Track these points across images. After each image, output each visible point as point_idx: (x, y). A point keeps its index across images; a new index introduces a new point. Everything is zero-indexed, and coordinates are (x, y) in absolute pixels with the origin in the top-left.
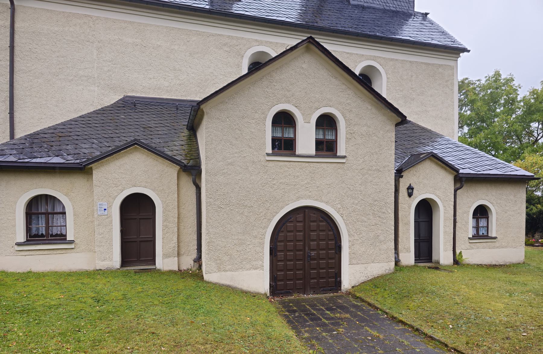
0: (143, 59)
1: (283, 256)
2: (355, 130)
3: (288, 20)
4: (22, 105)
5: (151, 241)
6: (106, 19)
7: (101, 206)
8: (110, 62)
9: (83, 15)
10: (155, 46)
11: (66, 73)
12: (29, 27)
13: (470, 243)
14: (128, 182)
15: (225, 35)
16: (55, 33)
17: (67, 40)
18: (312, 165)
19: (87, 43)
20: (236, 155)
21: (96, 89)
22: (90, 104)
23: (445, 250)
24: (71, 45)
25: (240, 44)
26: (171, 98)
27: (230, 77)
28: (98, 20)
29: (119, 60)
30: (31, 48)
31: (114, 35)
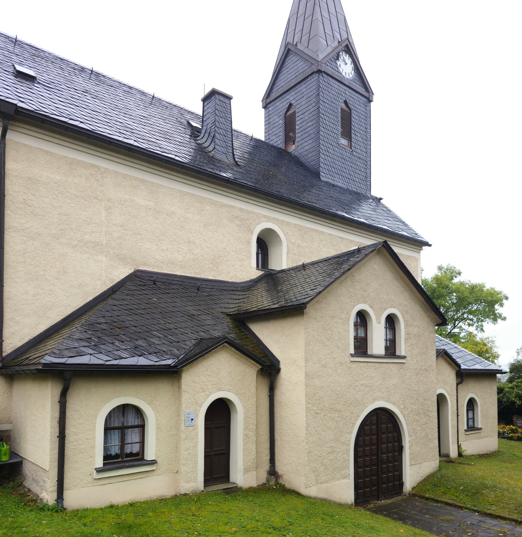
0: (156, 226)
1: (362, 462)
2: (411, 330)
3: (177, 158)
4: (12, 275)
5: (224, 453)
6: (116, 172)
7: (189, 416)
8: (121, 226)
9: (89, 163)
10: (170, 212)
11: (69, 236)
12: (23, 171)
13: (465, 435)
14: (214, 386)
15: (237, 207)
16: (56, 183)
17: (71, 194)
18: (383, 365)
19: (95, 201)
20: (328, 356)
21: (104, 259)
22: (97, 278)
23: (453, 444)
24: (76, 200)
25: (250, 219)
26: (185, 275)
27: (241, 254)
28: (106, 172)
29: (131, 226)
30: (26, 199)
31: (125, 194)
